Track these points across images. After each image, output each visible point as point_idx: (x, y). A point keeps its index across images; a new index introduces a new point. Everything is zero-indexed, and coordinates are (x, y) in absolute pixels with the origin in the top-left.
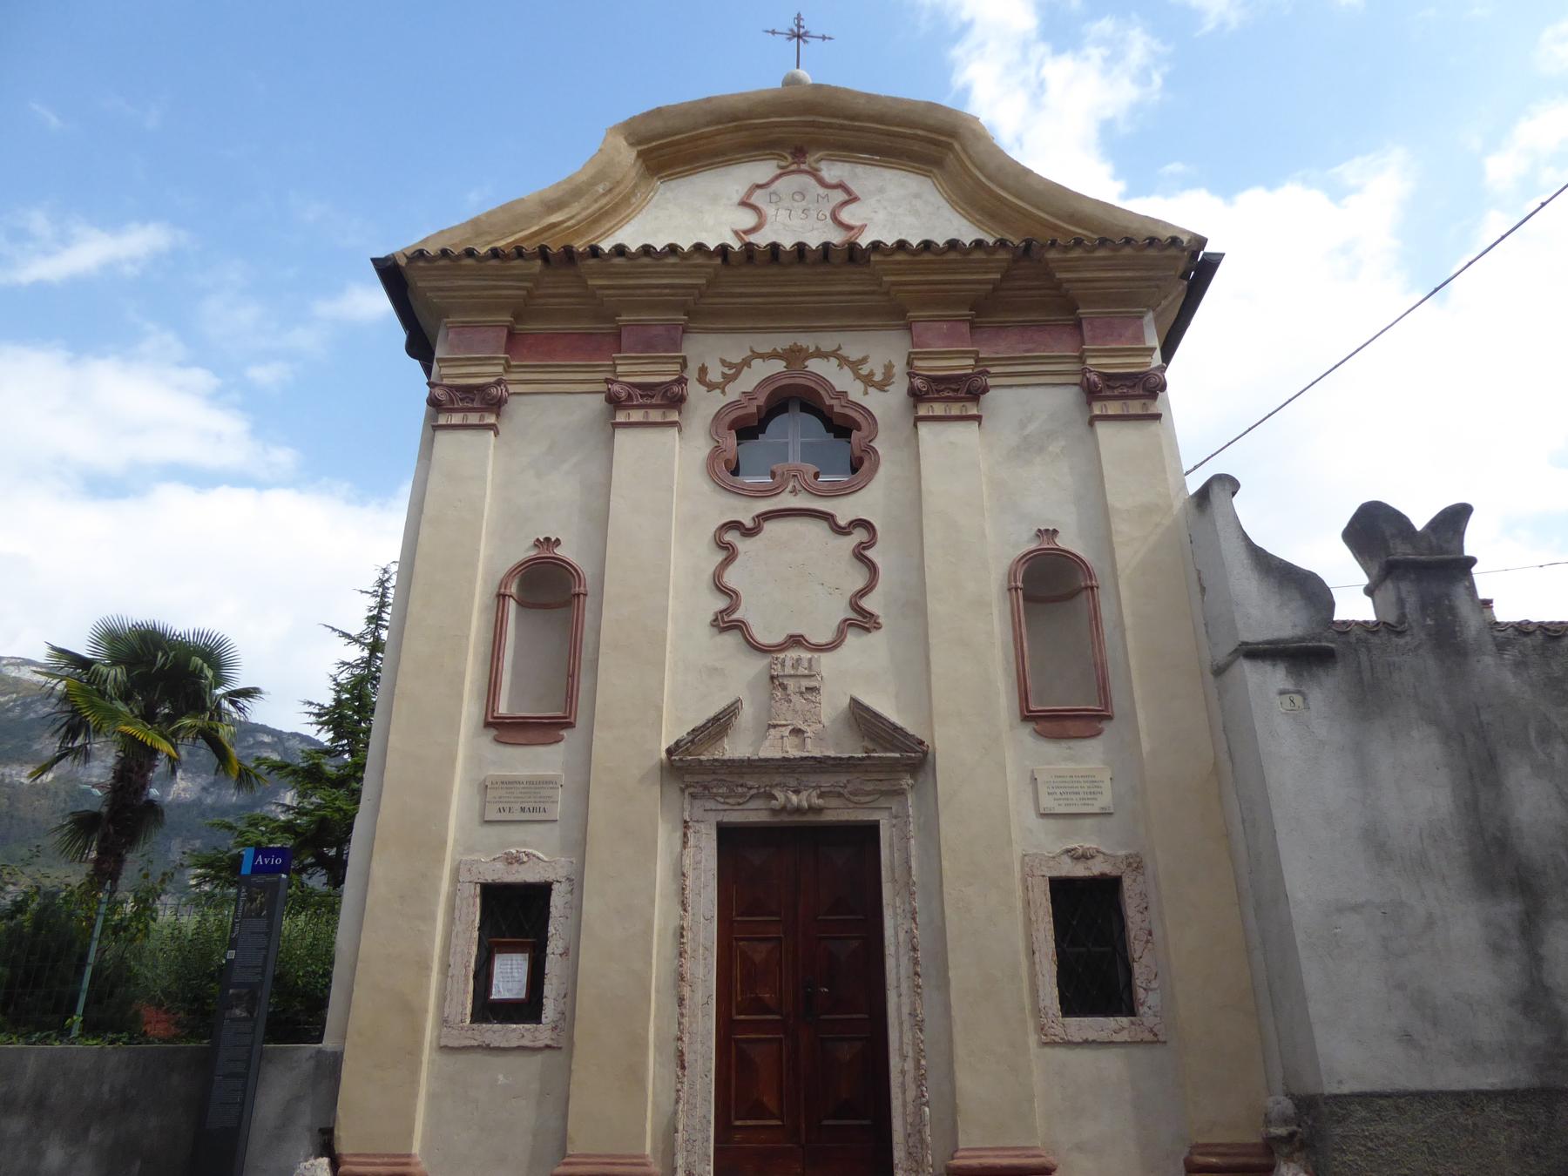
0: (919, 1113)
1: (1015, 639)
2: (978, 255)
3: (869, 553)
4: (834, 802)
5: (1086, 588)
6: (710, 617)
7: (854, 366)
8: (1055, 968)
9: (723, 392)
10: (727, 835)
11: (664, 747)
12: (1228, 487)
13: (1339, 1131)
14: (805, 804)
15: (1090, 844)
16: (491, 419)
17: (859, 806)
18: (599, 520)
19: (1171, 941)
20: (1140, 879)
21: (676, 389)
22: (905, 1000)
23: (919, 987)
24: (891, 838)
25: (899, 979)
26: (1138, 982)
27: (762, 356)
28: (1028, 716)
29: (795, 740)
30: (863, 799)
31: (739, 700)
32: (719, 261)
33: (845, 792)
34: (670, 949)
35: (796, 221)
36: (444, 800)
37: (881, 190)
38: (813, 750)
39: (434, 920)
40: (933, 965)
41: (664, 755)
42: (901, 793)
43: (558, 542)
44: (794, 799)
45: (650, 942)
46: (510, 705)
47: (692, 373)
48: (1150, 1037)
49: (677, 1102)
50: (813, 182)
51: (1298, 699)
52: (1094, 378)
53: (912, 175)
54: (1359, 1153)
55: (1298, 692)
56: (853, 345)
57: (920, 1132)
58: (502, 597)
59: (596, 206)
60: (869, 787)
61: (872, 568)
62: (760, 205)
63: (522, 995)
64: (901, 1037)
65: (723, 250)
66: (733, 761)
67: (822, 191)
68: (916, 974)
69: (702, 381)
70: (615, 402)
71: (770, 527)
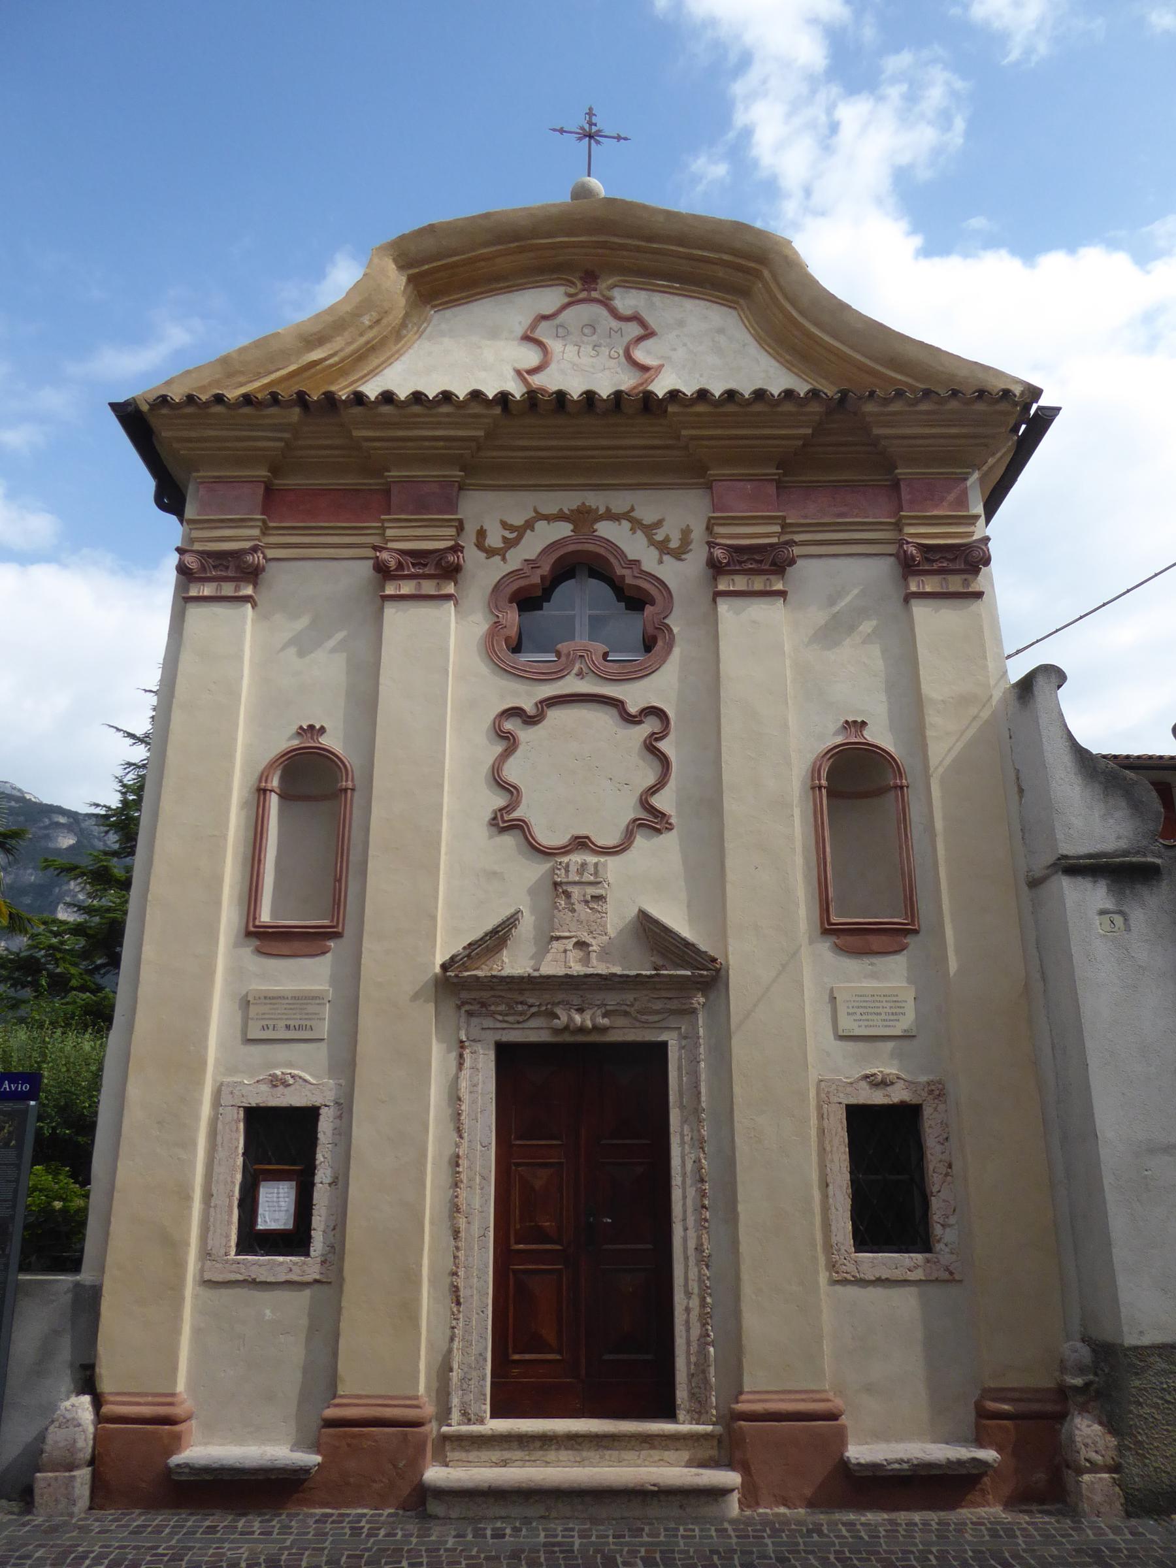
0: (702, 1352)
1: (817, 843)
2: (788, 407)
3: (663, 745)
4: (620, 1021)
5: (896, 787)
6: (488, 816)
7: (648, 530)
8: (848, 1203)
9: (504, 559)
10: (506, 1054)
11: (440, 959)
12: (1054, 680)
13: (1137, 1383)
14: (589, 1024)
15: (890, 1069)
16: (248, 591)
17: (646, 1025)
18: (365, 702)
19: (967, 1175)
20: (941, 1107)
21: (451, 558)
22: (692, 1234)
23: (706, 1220)
24: (680, 1059)
25: (685, 1212)
26: (935, 1218)
27: (548, 518)
28: (829, 930)
29: (579, 954)
30: (651, 1018)
31: (519, 911)
32: (498, 410)
33: (632, 1010)
34: (445, 1179)
35: (584, 367)
37: (681, 323)
38: (600, 967)
39: (194, 1144)
40: (723, 1201)
41: (438, 970)
42: (694, 1011)
43: (322, 730)
44: (578, 1018)
45: (423, 1173)
46: (274, 913)
47: (468, 541)
48: (946, 1276)
49: (452, 1339)
50: (604, 312)
51: (1118, 919)
52: (912, 550)
53: (715, 306)
54: (1156, 1406)
55: (1120, 912)
56: (648, 505)
57: (704, 1372)
58: (262, 792)
59: (362, 340)
60: (658, 1005)
61: (664, 761)
62: (544, 340)
63: (290, 1226)
64: (686, 1273)
65: (504, 398)
66: (513, 977)
67: (615, 324)
68: (704, 1207)
69: (480, 545)
70: (384, 572)
71: (555, 715)
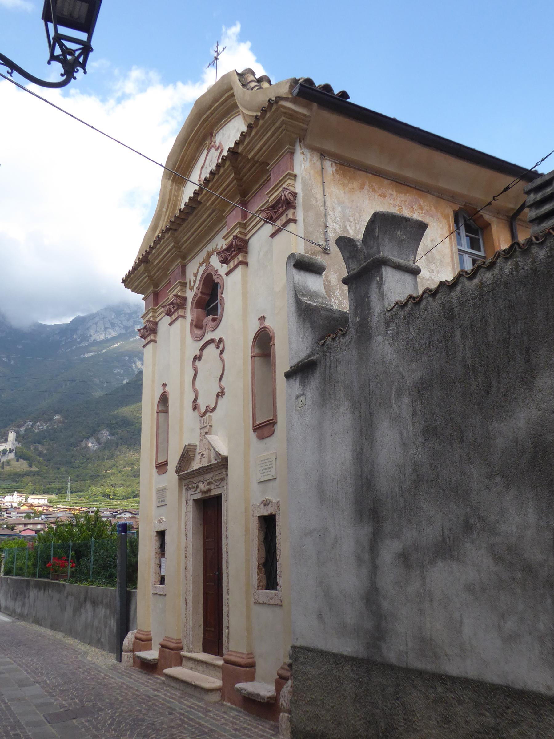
36: (18, 579)
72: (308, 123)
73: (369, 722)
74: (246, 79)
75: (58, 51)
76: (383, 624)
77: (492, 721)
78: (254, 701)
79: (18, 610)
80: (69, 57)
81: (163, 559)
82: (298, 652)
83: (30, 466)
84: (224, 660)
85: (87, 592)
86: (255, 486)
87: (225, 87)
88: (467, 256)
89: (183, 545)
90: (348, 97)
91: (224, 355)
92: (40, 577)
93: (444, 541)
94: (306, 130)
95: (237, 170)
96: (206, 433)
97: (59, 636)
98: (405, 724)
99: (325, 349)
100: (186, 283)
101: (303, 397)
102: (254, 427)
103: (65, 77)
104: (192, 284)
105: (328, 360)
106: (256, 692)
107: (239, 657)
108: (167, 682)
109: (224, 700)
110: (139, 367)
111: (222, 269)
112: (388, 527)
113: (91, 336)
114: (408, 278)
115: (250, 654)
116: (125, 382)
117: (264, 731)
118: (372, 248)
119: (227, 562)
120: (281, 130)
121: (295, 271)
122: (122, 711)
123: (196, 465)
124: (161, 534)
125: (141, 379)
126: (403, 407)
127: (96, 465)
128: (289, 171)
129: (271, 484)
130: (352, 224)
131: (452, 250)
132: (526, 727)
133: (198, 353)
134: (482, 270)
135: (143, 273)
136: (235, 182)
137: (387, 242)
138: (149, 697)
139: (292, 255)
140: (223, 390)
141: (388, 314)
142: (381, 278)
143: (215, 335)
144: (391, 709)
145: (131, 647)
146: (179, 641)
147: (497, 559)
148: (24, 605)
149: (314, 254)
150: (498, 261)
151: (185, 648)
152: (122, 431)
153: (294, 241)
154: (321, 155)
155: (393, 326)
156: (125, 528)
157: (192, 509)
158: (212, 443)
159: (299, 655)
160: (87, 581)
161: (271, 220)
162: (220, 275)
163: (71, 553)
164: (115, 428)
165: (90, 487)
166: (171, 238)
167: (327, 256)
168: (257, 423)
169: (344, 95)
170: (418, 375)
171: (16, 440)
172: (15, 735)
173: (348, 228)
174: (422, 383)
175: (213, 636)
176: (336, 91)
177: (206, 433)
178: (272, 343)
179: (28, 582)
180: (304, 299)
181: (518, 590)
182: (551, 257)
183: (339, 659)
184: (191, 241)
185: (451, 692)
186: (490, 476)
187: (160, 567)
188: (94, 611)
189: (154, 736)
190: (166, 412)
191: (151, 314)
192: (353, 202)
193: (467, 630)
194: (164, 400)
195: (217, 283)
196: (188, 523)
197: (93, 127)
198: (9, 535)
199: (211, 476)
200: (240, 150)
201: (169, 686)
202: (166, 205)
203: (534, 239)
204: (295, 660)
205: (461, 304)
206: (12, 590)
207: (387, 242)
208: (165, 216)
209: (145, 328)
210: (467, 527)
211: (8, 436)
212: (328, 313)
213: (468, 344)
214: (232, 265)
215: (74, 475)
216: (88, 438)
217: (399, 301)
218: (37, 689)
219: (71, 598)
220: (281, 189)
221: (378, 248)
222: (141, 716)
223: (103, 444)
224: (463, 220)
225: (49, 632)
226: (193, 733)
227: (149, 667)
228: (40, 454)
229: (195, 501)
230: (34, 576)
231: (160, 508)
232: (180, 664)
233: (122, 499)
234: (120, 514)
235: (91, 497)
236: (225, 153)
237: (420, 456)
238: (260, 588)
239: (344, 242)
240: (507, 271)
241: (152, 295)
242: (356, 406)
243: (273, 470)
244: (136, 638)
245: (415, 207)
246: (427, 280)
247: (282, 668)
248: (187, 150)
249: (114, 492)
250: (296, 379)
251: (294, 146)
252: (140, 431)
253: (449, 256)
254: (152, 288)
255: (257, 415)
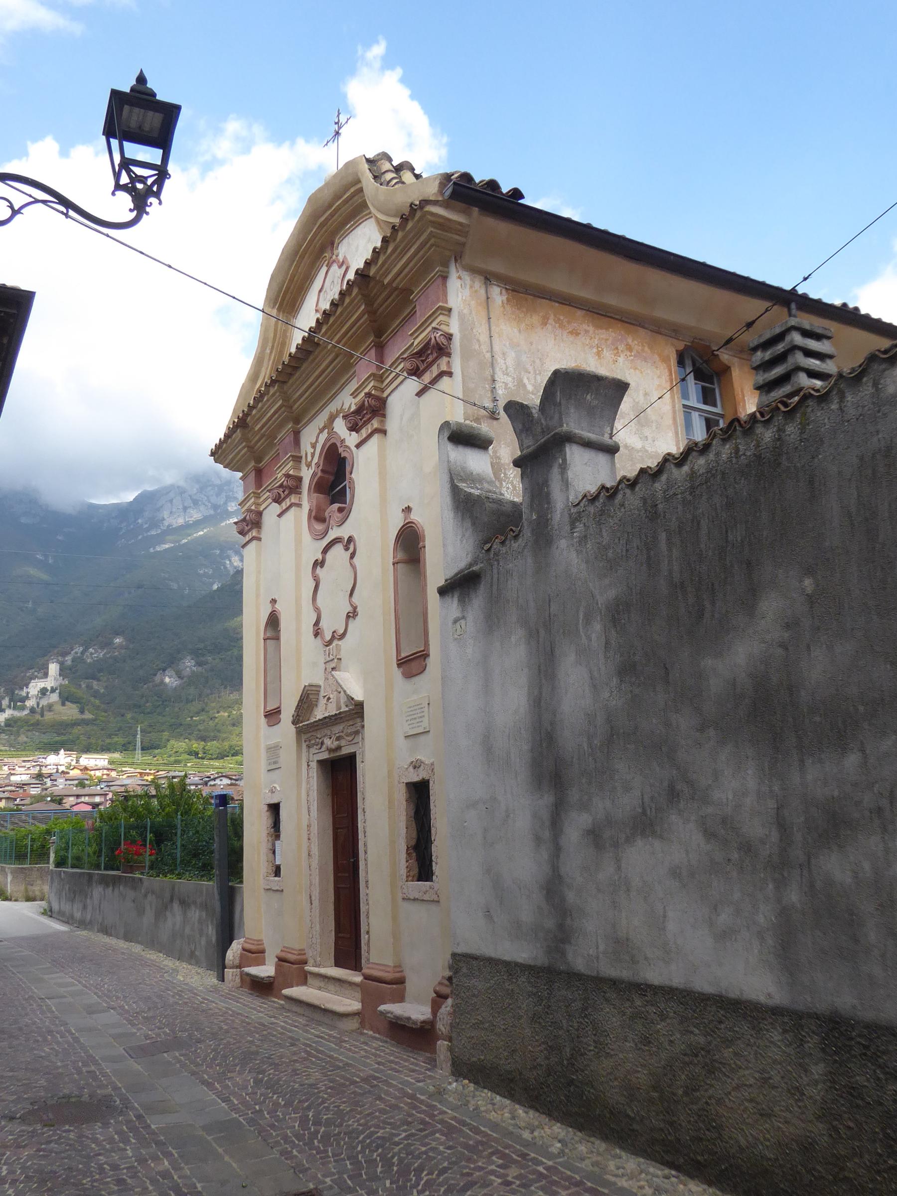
72: (465, 234)
73: (550, 1047)
74: (379, 168)
75: (124, 179)
76: (568, 921)
77: (702, 1040)
78: (403, 1027)
79: (78, 915)
80: (140, 186)
81: (277, 843)
82: (459, 961)
83: (82, 712)
84: (363, 975)
85: (173, 889)
86: (401, 741)
87: (350, 179)
88: (697, 414)
89: (305, 823)
90: (522, 197)
91: (355, 560)
92: (106, 869)
93: (644, 813)
94: (464, 244)
95: (369, 300)
96: (333, 669)
97: (137, 948)
98: (595, 1047)
99: (492, 556)
100: (301, 457)
101: (463, 622)
102: (398, 660)
103: (135, 212)
104: (309, 459)
105: (495, 571)
106: (406, 1015)
107: (383, 970)
108: (287, 1006)
109: (364, 1028)
110: (235, 564)
111: (351, 439)
112: (574, 795)
113: (164, 519)
114: (602, 459)
115: (398, 967)
116: (215, 587)
117: (417, 1065)
118: (551, 418)
119: (365, 845)
120: (428, 245)
121: (450, 447)
122: (228, 1042)
123: (319, 713)
124: (275, 808)
125: (240, 583)
126: (594, 636)
127: (176, 709)
128: (440, 304)
129: (422, 738)
130: (531, 376)
131: (674, 407)
132: (742, 1046)
133: (320, 557)
134: (694, 454)
135: (240, 443)
136: (366, 316)
137: (572, 411)
138: (264, 1025)
139: (446, 424)
140: (355, 608)
141: (574, 510)
142: (564, 460)
143: (343, 532)
144: (577, 1030)
145: (237, 962)
146: (302, 952)
147: (709, 835)
148: (85, 907)
149: (477, 420)
150: (714, 442)
151: (311, 961)
152: (214, 659)
153: (448, 403)
154: (486, 278)
155: (580, 527)
156: (223, 800)
157: (315, 774)
158: (342, 683)
159: (461, 964)
160: (173, 873)
161: (416, 372)
162: (347, 447)
163: (149, 836)
164: (203, 655)
165: (168, 741)
166: (278, 394)
167: (495, 422)
168: (403, 655)
169: (517, 194)
170: (612, 593)
171: (60, 675)
172: (88, 1072)
173: (526, 381)
174: (618, 605)
175: (348, 946)
176: (505, 189)
177: (333, 669)
178: (421, 544)
179: (90, 876)
180: (462, 485)
181: (734, 874)
182: (779, 439)
183: (511, 968)
184: (306, 398)
185: (652, 1005)
186: (702, 729)
187: (274, 852)
188: (185, 913)
189: (272, 1071)
190: (277, 638)
191: (253, 500)
192: (531, 344)
193: (672, 926)
194: (273, 621)
195: (344, 459)
196: (311, 793)
197: (170, 266)
198: (56, 812)
199: (341, 728)
200: (372, 272)
201: (289, 1011)
202: (270, 345)
203: (758, 415)
204: (456, 973)
205: (667, 499)
206: (67, 887)
207: (572, 411)
208: (269, 360)
209: (244, 520)
210: (673, 795)
211: (48, 668)
212: (495, 506)
213: (676, 553)
214: (364, 433)
215: (146, 723)
216: (164, 670)
217: (589, 492)
218: (112, 1017)
219: (150, 897)
220: (430, 328)
221: (561, 418)
222: (254, 1048)
223: (185, 679)
224: (690, 362)
225: (122, 944)
226: (324, 1068)
227: (262, 988)
228: (96, 694)
229: (321, 763)
230: (98, 867)
231: (271, 773)
232: (304, 982)
233: (216, 759)
234: (214, 779)
235: (170, 756)
236: (351, 276)
237: (614, 702)
238: (410, 878)
239: (516, 410)
240: (724, 456)
241: (253, 474)
242: (532, 635)
243: (426, 720)
244: (244, 949)
245: (621, 347)
246: (638, 451)
247: (440, 983)
248: (298, 266)
249: (204, 748)
250: (453, 597)
251: (448, 267)
252: (240, 658)
253: (670, 415)
254: (252, 464)
255: (402, 646)
